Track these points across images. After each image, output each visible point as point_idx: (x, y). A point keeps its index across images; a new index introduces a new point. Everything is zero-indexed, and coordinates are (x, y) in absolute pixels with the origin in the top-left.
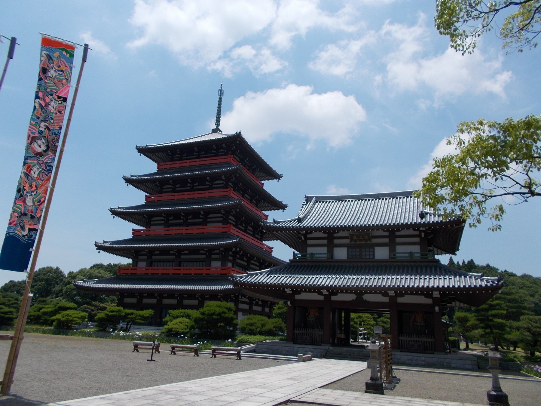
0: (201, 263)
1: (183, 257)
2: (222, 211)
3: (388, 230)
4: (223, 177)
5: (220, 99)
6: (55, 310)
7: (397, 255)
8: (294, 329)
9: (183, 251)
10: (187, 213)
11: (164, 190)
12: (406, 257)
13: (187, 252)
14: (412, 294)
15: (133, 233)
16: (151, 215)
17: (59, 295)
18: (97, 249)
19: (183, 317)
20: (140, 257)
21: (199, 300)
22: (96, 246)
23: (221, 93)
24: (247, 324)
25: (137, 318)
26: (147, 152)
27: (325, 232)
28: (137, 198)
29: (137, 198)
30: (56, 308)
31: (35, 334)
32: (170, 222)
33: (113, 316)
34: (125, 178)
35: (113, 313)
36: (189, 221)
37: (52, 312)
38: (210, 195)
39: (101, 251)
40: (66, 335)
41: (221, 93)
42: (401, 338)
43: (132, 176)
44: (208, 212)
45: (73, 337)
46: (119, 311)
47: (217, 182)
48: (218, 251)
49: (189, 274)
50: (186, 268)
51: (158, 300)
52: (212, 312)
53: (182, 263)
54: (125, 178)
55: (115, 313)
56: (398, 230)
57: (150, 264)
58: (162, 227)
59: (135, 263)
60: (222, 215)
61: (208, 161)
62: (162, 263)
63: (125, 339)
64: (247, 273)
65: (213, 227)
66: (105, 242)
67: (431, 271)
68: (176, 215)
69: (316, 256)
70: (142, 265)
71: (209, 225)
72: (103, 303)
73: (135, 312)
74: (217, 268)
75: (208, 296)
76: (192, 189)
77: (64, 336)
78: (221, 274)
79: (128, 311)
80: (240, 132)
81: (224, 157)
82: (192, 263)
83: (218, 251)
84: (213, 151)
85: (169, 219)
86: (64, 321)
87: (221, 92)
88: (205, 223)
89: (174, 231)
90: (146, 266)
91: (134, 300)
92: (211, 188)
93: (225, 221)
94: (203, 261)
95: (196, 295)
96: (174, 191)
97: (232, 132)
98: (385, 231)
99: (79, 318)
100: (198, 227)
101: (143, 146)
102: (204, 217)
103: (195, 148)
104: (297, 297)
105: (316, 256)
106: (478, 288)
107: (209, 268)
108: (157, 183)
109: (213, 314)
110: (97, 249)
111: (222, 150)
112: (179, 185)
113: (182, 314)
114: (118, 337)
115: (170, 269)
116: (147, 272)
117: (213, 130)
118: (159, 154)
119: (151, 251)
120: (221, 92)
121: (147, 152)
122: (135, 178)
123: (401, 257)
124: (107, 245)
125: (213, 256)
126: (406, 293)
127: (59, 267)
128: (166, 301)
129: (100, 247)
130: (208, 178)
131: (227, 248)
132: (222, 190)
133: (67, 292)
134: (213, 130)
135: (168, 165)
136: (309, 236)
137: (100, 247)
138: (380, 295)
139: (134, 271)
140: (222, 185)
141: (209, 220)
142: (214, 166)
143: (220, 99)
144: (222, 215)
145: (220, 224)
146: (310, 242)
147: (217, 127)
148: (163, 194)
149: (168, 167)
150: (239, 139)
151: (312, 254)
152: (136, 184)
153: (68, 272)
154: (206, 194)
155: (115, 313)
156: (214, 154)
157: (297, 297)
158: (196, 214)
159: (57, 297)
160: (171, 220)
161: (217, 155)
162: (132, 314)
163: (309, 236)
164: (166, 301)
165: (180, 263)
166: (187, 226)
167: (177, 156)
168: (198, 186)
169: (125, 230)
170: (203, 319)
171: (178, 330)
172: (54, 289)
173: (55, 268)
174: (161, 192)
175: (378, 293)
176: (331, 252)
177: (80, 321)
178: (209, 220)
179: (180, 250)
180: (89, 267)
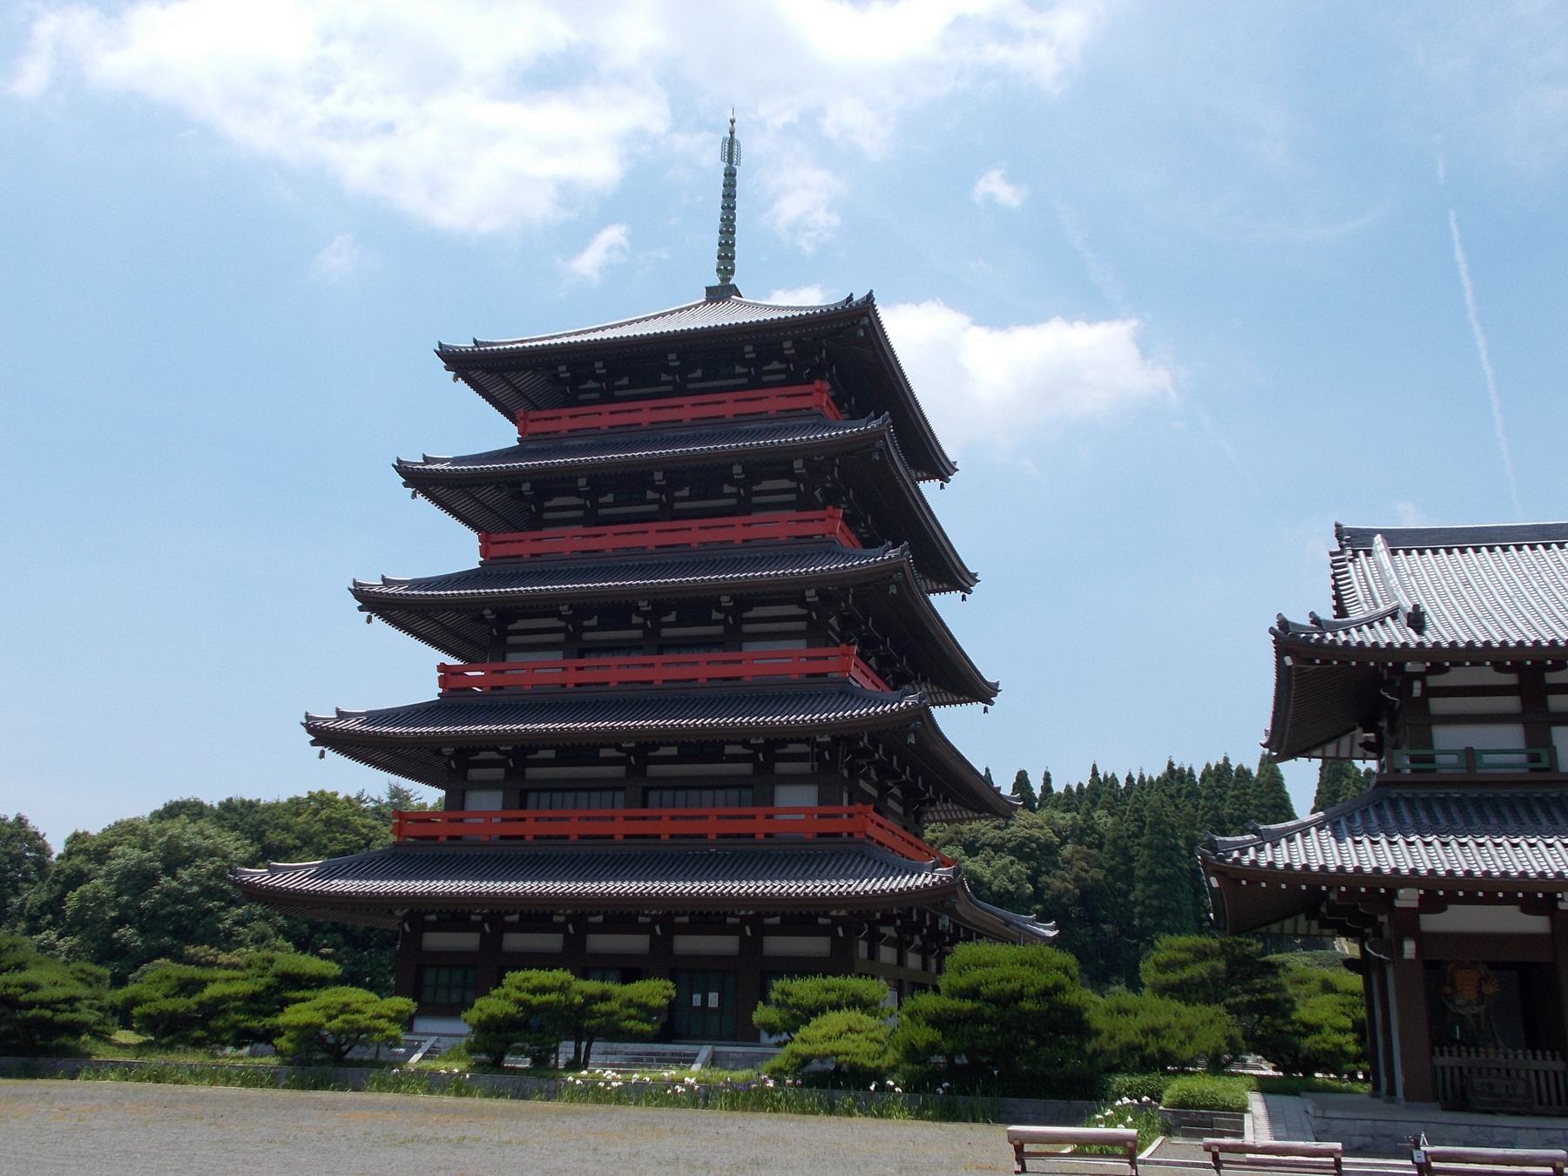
0: (609, 794)
1: (532, 772)
2: (487, 612)
3: (1517, 667)
4: (798, 464)
5: (730, 175)
6: (268, 987)
7: (1441, 759)
8: (1433, 1053)
9: (535, 750)
10: (661, 603)
11: (547, 516)
12: (1512, 766)
13: (551, 754)
14: (1470, 899)
15: (443, 682)
16: (508, 612)
17: (43, 922)
18: (313, 743)
19: (836, 1007)
20: (475, 774)
21: (834, 935)
22: (306, 726)
23: (730, 154)
24: (1145, 1033)
25: (625, 1012)
26: (478, 367)
27: (1499, 667)
28: (448, 548)
29: (448, 548)
30: (268, 980)
31: (204, 1089)
32: (587, 636)
33: (547, 1007)
34: (402, 468)
35: (546, 998)
36: (666, 632)
37: (254, 997)
38: (537, 548)
39: (329, 752)
40: (356, 1089)
41: (730, 154)
42: (1440, 1061)
43: (427, 460)
44: (746, 598)
45: (388, 1097)
46: (563, 988)
47: (767, 485)
48: (493, 755)
49: (560, 837)
50: (550, 814)
51: (484, 937)
52: (1016, 985)
53: (532, 797)
54: (402, 468)
55: (553, 997)
56: (1437, 669)
57: (520, 795)
58: (557, 656)
59: (455, 801)
60: (561, 624)
61: (645, 414)
62: (668, 795)
63: (619, 1101)
64: (1256, 832)
65: (774, 656)
66: (341, 715)
67: (1537, 822)
68: (615, 611)
69: (1487, 758)
70: (486, 802)
71: (750, 647)
72: (228, 951)
73: (615, 988)
74: (488, 815)
75: (686, 919)
76: (668, 513)
77: (349, 1095)
78: (503, 837)
79: (593, 986)
80: (441, 345)
81: (741, 395)
82: (569, 797)
83: (493, 755)
84: (739, 369)
85: (584, 625)
86: (337, 1033)
87: (731, 149)
88: (732, 639)
89: (613, 670)
90: (505, 807)
91: (637, 943)
92: (744, 508)
93: (815, 634)
94: (740, 787)
95: (471, 912)
96: (592, 519)
97: (811, 297)
98: (1507, 670)
99: (391, 1020)
100: (621, 659)
101: (465, 343)
102: (726, 618)
103: (672, 356)
104: (1431, 923)
105: (1487, 758)
106: (1422, 878)
107: (768, 810)
108: (526, 487)
109: (1019, 996)
110: (313, 743)
111: (775, 365)
112: (619, 493)
113: (833, 997)
114: (596, 1094)
115: (615, 819)
116: (515, 828)
117: (710, 290)
118: (524, 380)
119: (522, 751)
120: (731, 149)
121: (478, 367)
122: (438, 466)
123: (1499, 766)
124: (352, 725)
125: (782, 767)
126: (1451, 898)
127: (26, 814)
128: (776, 945)
129: (326, 736)
130: (658, 476)
131: (843, 737)
132: (579, 529)
133: (81, 910)
134: (710, 290)
135: (565, 421)
136: (1433, 681)
137: (326, 736)
138: (1513, 910)
139: (455, 830)
140: (580, 513)
141: (512, 640)
142: (709, 431)
143: (730, 175)
144: (561, 624)
145: (800, 645)
146: (1438, 705)
147: (725, 279)
148: (547, 532)
149: (565, 425)
150: (866, 321)
151: (1470, 754)
152: (440, 491)
153: (68, 833)
154: (735, 530)
155: (553, 997)
156: (669, 388)
157: (1431, 923)
158: (695, 606)
159: (33, 930)
160: (592, 629)
161: (755, 383)
162: (605, 997)
163: (1433, 681)
164: (776, 945)
165: (646, 792)
166: (581, 656)
167: (591, 384)
168: (615, 504)
169: (409, 672)
170: (975, 1017)
171: (856, 1059)
172: (16, 901)
173: (11, 819)
174: (536, 522)
175: (1501, 902)
176: (1539, 740)
177: (395, 1030)
178: (747, 628)
179: (644, 748)
180: (147, 815)
